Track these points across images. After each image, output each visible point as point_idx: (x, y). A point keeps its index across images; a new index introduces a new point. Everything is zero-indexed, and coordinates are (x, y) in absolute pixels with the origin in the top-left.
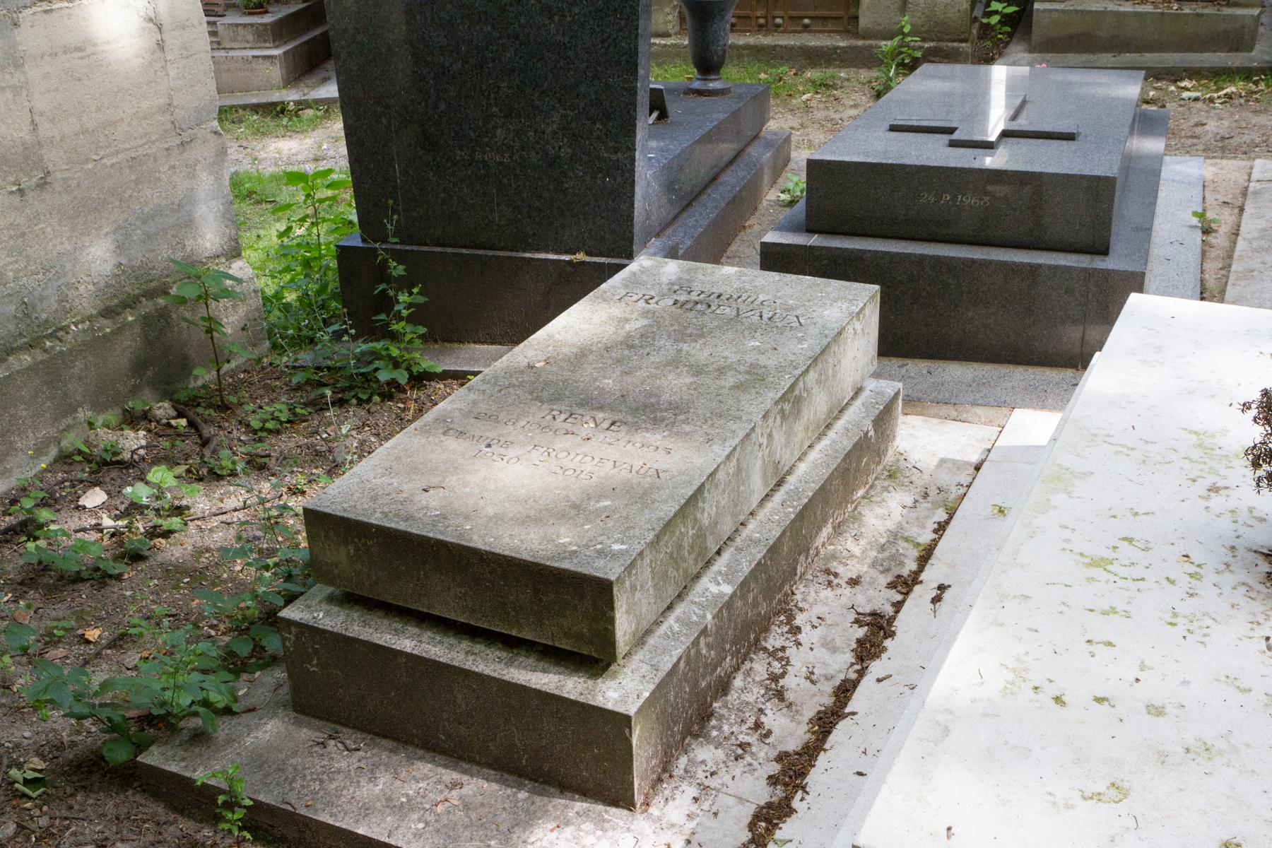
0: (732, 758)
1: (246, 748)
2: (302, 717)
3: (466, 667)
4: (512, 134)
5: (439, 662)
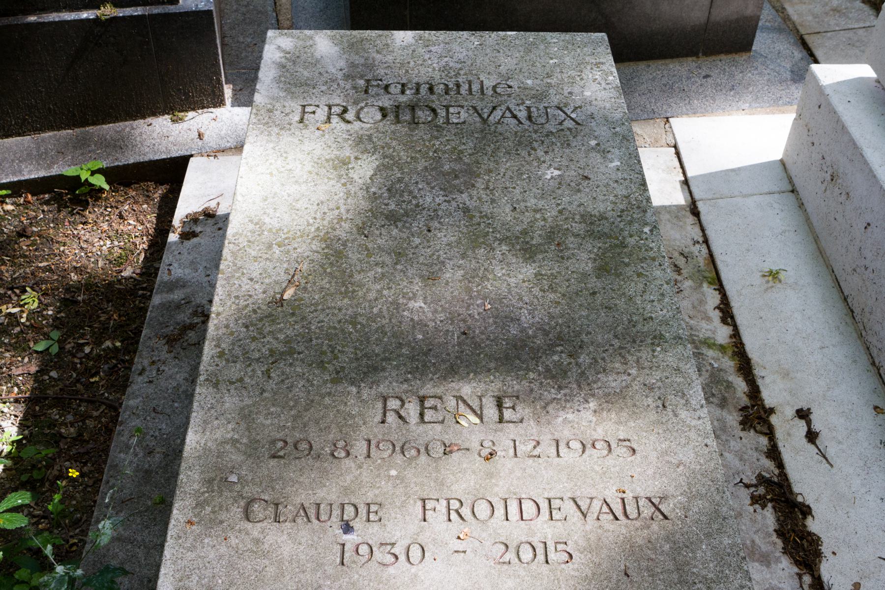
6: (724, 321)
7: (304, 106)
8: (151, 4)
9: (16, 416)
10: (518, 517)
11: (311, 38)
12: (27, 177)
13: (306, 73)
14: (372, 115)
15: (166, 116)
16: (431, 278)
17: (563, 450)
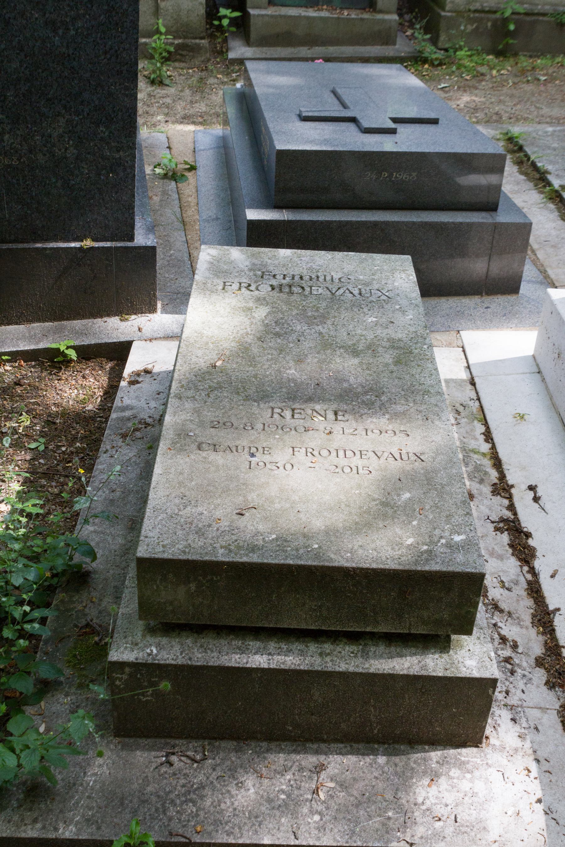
0: (509, 674)
1: (92, 788)
2: (127, 740)
3: (330, 669)
4: (19, 139)
5: (301, 670)
6: (486, 441)
7: (225, 282)
8: (116, 241)
9: (19, 481)
10: (344, 456)
11: (228, 250)
12: (22, 349)
13: (225, 267)
14: (265, 288)
15: (117, 317)
16: (299, 361)
17: (369, 433)
